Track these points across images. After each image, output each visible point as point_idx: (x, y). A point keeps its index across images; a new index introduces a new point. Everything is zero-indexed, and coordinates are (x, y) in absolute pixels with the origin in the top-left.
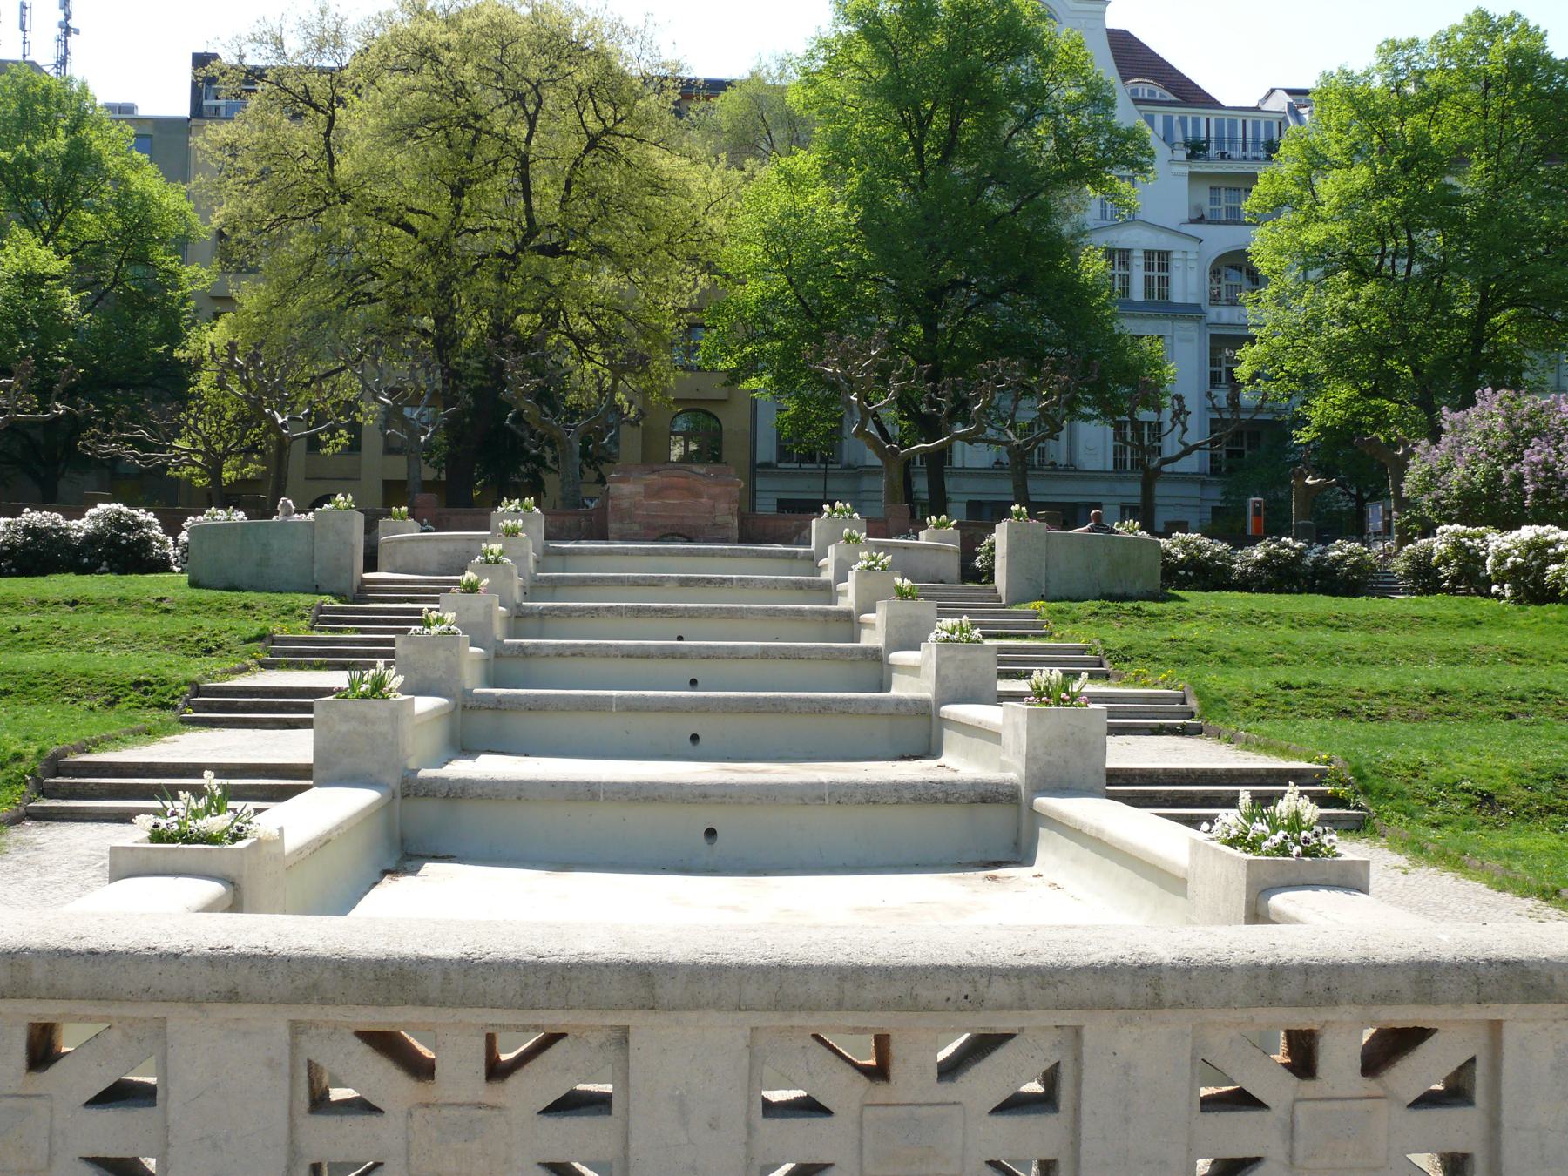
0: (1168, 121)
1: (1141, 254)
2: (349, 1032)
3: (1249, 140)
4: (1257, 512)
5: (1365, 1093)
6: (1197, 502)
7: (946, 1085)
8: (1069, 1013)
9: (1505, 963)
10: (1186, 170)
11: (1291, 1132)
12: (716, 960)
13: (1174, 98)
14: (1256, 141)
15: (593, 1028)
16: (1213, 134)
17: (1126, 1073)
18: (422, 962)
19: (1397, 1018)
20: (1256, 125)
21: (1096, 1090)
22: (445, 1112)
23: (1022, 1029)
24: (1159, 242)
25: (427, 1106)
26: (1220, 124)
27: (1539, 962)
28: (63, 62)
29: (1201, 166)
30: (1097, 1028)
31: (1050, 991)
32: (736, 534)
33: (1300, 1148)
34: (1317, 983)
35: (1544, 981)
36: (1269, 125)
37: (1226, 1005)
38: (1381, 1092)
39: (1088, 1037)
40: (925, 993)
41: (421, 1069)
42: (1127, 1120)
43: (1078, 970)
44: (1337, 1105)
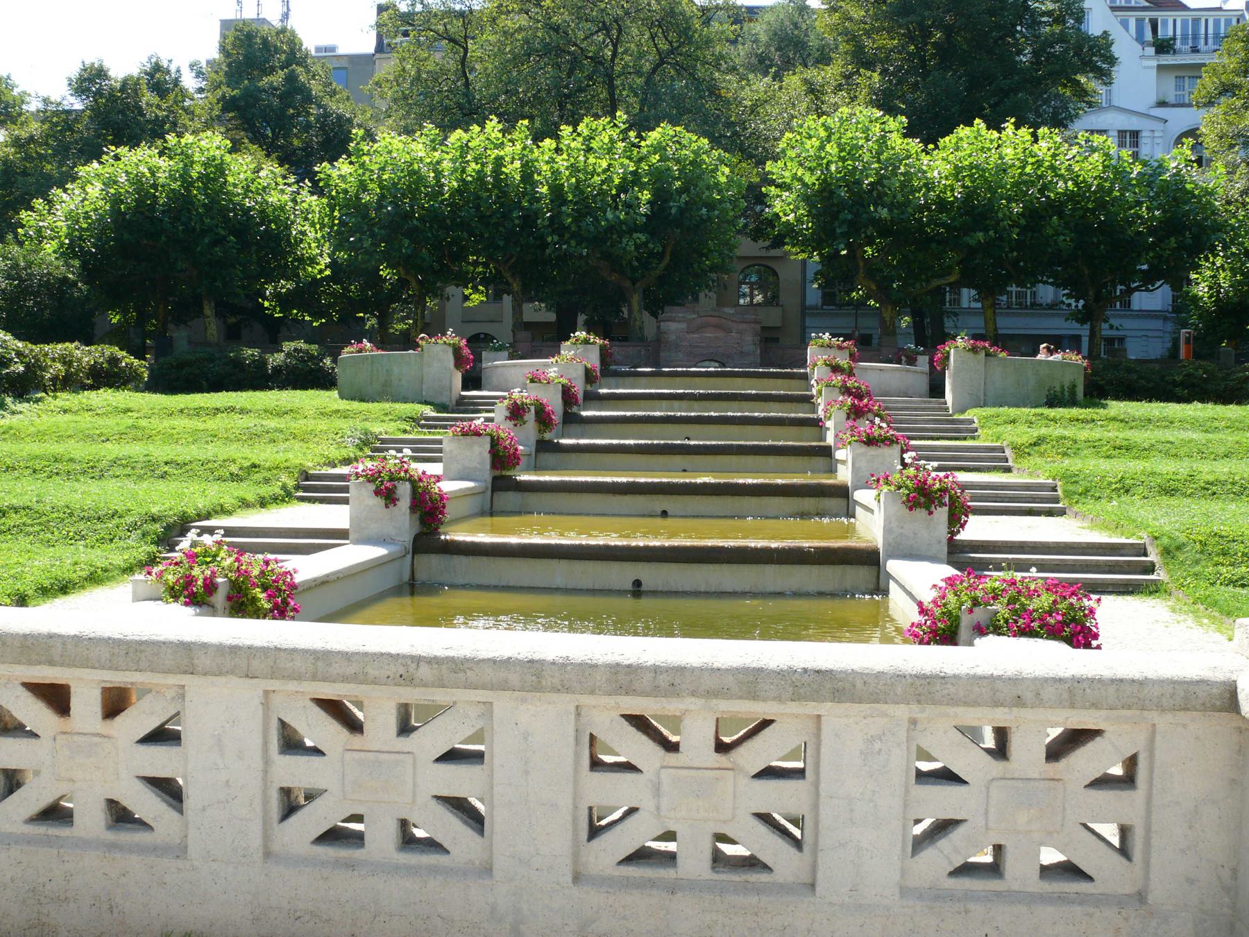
0: (1140, 21)
1: (1116, 134)
2: (17, 683)
3: (1210, 36)
4: (1188, 341)
5: (717, 765)
6: (1160, 334)
7: (401, 739)
8: (481, 692)
9: (818, 672)
10: (1155, 63)
11: (657, 790)
12: (235, 642)
13: (1147, 4)
14: (1216, 35)
15: (169, 687)
16: (1179, 32)
17: (526, 738)
18: (51, 636)
19: (37, 674)
20: (1217, 23)
21: (501, 749)
22: (76, 738)
23: (455, 703)
24: (1132, 123)
25: (65, 733)
26: (1185, 23)
27: (845, 672)
28: (286, 16)
29: (1168, 60)
30: (503, 703)
31: (461, 675)
32: (758, 360)
33: (665, 803)
34: (663, 680)
35: (848, 686)
36: (1228, 22)
37: (592, 692)
38: (730, 766)
39: (497, 712)
40: (372, 672)
41: (354, 726)
42: (527, 773)
43: (483, 660)
44: (693, 773)
